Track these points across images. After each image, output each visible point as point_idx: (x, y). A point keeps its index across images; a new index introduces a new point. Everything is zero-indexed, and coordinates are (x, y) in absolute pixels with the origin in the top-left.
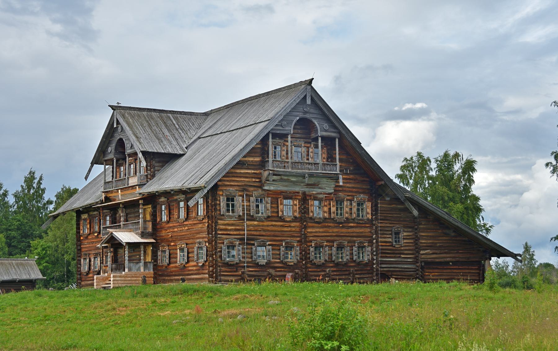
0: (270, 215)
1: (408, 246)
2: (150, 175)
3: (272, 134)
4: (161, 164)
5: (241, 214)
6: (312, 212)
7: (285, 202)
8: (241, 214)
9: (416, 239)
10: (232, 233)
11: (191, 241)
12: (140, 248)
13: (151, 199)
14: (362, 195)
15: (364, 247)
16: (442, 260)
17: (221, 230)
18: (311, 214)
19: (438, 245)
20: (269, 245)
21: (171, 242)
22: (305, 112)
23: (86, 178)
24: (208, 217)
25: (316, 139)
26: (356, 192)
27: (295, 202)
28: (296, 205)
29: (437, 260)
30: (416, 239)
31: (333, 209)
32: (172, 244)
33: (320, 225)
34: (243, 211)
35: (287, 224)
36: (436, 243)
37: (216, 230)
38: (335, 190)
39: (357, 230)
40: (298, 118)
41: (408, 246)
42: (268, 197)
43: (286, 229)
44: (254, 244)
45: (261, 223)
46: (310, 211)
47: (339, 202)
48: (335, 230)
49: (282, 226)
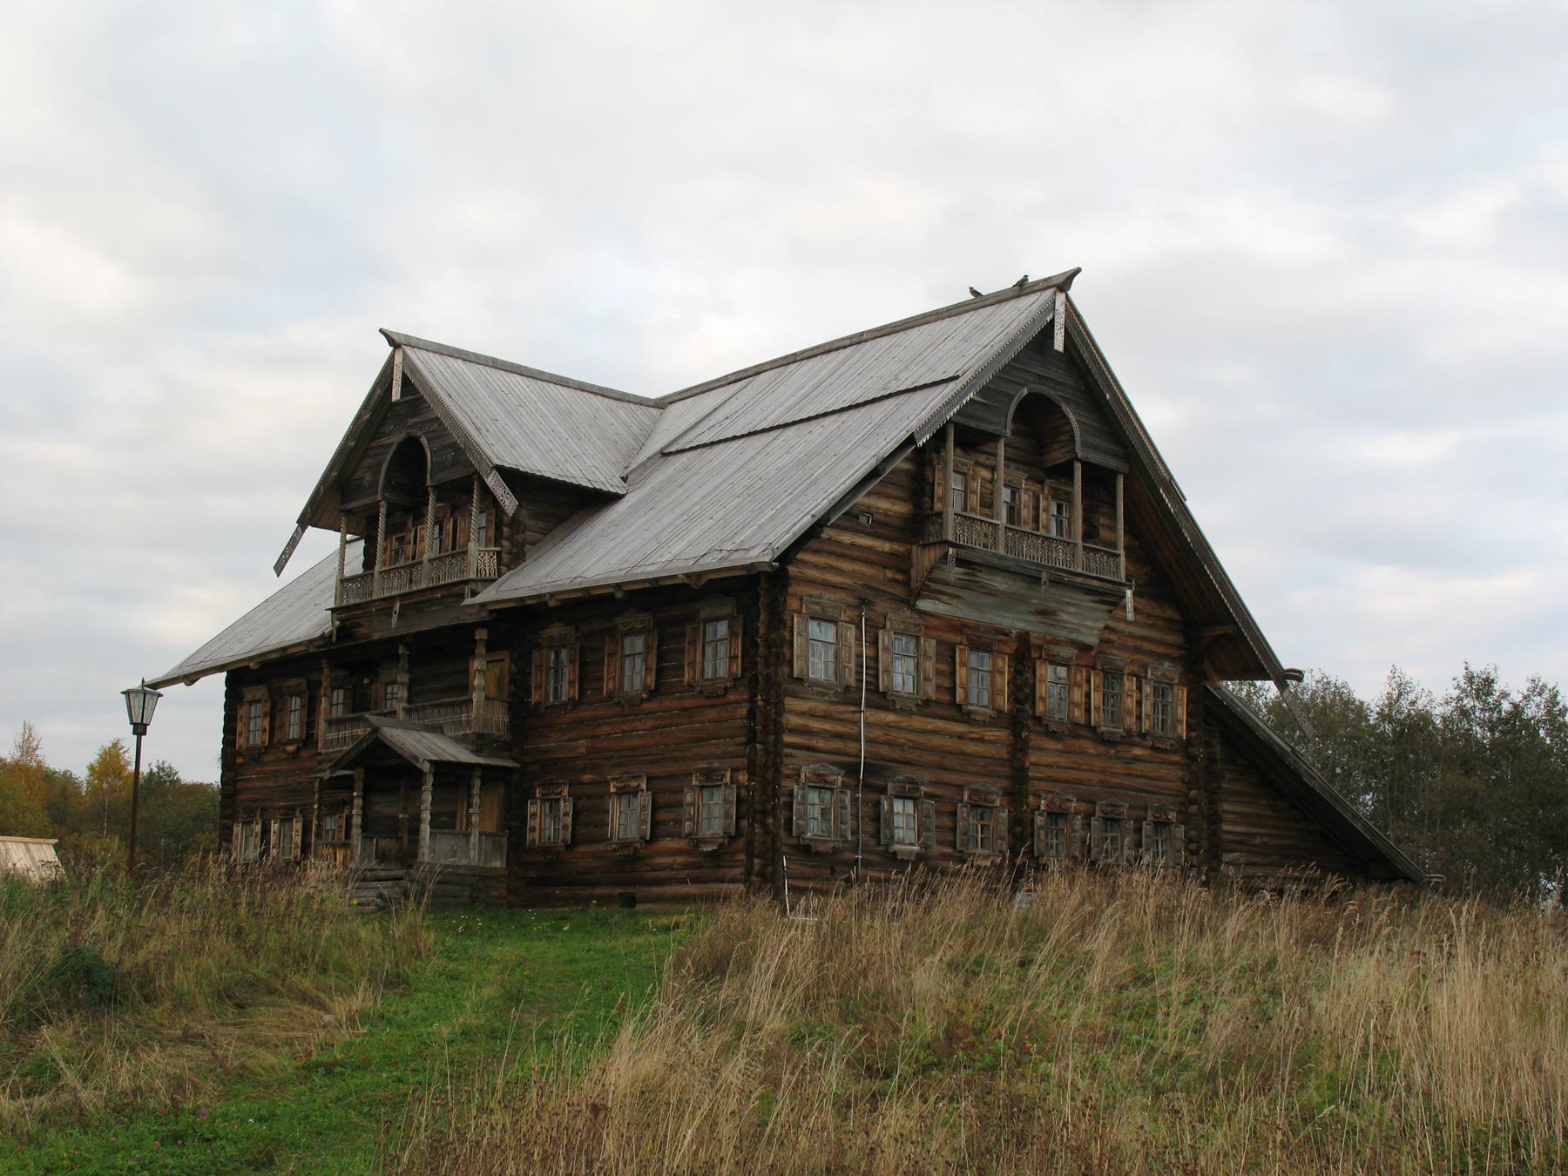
2: (510, 553)
4: (541, 524)
5: (853, 683)
8: (853, 683)
10: (821, 744)
11: (672, 768)
12: (470, 788)
13: (521, 623)
14: (1166, 664)
18: (1040, 707)
19: (1258, 841)
20: (928, 796)
21: (584, 770)
22: (1041, 379)
23: (279, 568)
24: (754, 682)
25: (1064, 472)
26: (1151, 653)
27: (1000, 663)
31: (1096, 698)
32: (587, 777)
34: (859, 673)
35: (976, 732)
36: (1252, 835)
37: (779, 729)
39: (1149, 769)
40: (1025, 391)
42: (928, 636)
43: (971, 748)
44: (883, 790)
47: (1112, 675)
48: (1098, 763)
49: (961, 737)
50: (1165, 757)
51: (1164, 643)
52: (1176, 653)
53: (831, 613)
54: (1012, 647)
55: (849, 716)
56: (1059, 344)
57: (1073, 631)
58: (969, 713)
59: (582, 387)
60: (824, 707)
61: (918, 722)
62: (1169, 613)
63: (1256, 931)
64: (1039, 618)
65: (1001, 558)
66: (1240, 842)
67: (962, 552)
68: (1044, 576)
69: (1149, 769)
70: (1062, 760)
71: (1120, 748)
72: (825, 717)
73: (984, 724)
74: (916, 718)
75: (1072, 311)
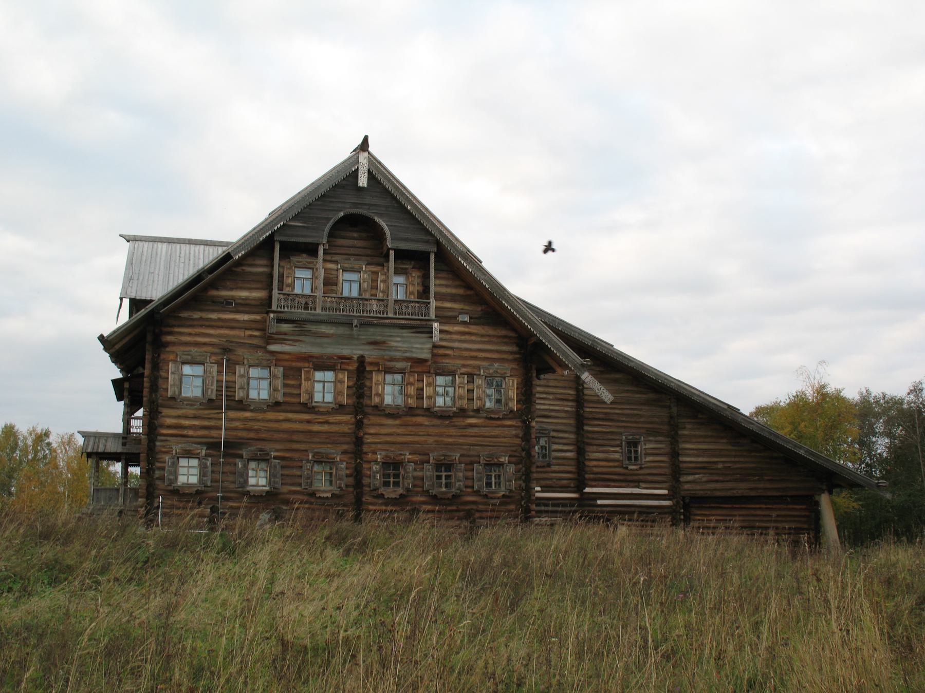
0: (280, 398)
1: (655, 467)
3: (282, 244)
6: (378, 395)
7: (318, 375)
9: (675, 454)
10: (191, 433)
15: (501, 465)
16: (729, 493)
17: (169, 427)
25: (387, 256)
27: (340, 376)
28: (342, 382)
29: (718, 494)
30: (675, 454)
33: (397, 422)
35: (321, 418)
36: (716, 463)
38: (434, 355)
39: (483, 431)
40: (342, 214)
41: (655, 467)
43: (316, 428)
45: (260, 416)
46: (373, 392)
48: (432, 430)
49: (309, 422)
50: (499, 422)
51: (497, 351)
52: (510, 357)
53: (198, 359)
54: (353, 367)
55: (215, 416)
56: (363, 181)
57: (406, 351)
58: (313, 407)
59: (190, 242)
60: (193, 412)
61: (271, 415)
62: (503, 332)
63: (594, 531)
64: (372, 347)
65: (319, 315)
66: (704, 468)
67: (280, 315)
68: (355, 322)
69: (483, 431)
70: (400, 430)
71: (455, 420)
72: (195, 417)
73: (328, 413)
74: (269, 413)
75: (374, 163)
